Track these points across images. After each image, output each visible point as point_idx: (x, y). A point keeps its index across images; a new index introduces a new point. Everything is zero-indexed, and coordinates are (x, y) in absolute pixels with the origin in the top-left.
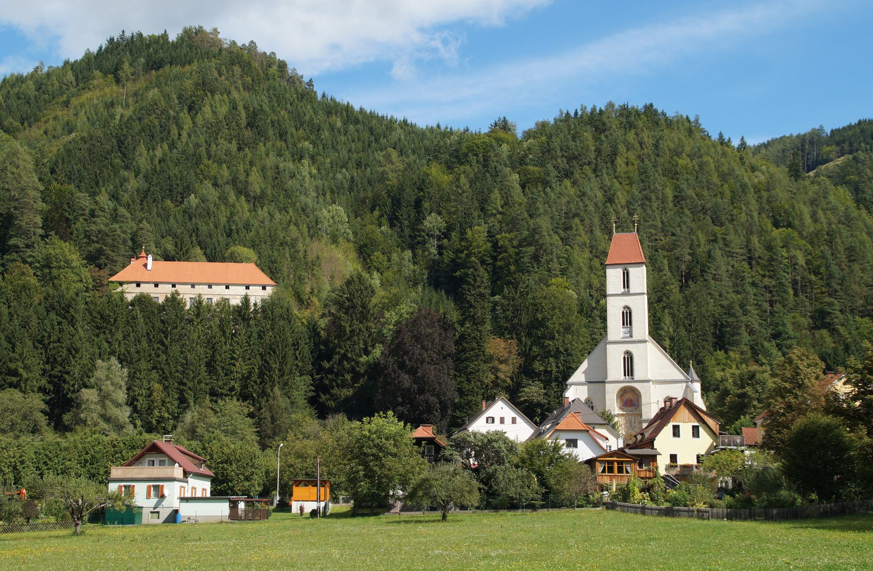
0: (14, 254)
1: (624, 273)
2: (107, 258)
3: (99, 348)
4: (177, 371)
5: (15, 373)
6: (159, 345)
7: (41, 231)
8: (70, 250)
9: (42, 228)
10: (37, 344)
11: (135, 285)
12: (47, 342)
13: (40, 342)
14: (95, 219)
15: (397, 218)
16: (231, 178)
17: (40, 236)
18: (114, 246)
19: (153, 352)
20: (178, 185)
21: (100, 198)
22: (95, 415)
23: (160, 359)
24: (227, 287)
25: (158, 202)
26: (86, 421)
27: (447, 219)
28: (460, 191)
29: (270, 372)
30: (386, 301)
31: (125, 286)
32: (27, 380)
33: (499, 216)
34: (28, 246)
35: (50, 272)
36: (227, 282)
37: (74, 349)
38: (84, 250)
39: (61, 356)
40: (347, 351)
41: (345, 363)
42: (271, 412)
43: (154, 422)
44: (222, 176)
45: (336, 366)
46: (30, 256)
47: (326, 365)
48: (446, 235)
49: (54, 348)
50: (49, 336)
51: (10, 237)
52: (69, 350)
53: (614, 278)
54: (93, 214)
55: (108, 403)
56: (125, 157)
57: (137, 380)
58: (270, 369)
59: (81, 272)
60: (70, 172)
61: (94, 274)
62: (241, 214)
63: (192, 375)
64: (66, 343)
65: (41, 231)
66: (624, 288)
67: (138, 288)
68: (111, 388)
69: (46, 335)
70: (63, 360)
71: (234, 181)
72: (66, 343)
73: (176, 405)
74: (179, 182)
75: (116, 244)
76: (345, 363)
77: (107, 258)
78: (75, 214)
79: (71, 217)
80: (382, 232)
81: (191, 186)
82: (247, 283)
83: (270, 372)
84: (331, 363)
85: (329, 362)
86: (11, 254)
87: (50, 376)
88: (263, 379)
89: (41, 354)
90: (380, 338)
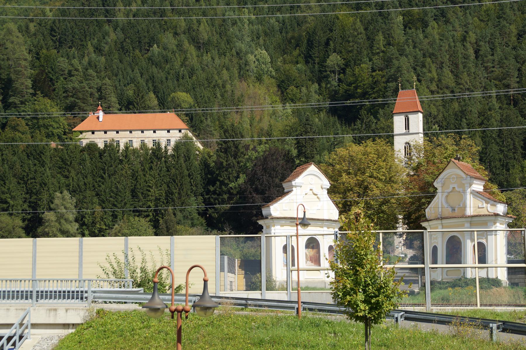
0: (13, 109)
1: (406, 119)
2: (79, 108)
3: (59, 183)
4: (111, 197)
5: (6, 202)
6: (100, 179)
7: (31, 91)
8: (51, 106)
9: (32, 88)
10: (20, 181)
11: (91, 133)
12: (26, 179)
13: (22, 180)
14: (72, 78)
15: (310, 57)
16: (187, 28)
17: (31, 94)
18: (84, 99)
19: (95, 184)
20: (145, 37)
21: (75, 61)
22: (55, 229)
23: (101, 188)
24: (154, 132)
25: (129, 52)
26: (49, 233)
27: (345, 57)
28: (356, 33)
29: (172, 195)
30: (288, 128)
31: (84, 134)
32: (13, 206)
33: (381, 54)
34: (22, 103)
35: (38, 122)
36: (154, 128)
37: (44, 183)
38: (63, 103)
39: (35, 189)
40: (224, 179)
41: (223, 187)
42: (166, 224)
43: (96, 231)
44: (180, 27)
45: (218, 189)
46: (24, 111)
47: (212, 189)
48: (343, 71)
49: (31, 183)
50: (28, 175)
51: (10, 97)
52: (41, 185)
53: (398, 122)
54: (70, 74)
55: (63, 221)
56: (108, 13)
57: (85, 204)
58: (172, 194)
59: (59, 120)
60: (65, 29)
61: (70, 121)
62: (190, 60)
63: (120, 200)
64: (38, 180)
65: (31, 91)
66: (406, 129)
67: (93, 135)
68: (64, 211)
69: (25, 174)
70: (37, 191)
71: (189, 29)
72: (38, 180)
73: (111, 220)
74: (146, 34)
75: (85, 97)
76: (223, 187)
77: (79, 108)
78: (57, 75)
79: (54, 78)
80: (298, 69)
81: (155, 37)
82: (168, 128)
83: (172, 195)
84: (215, 187)
85: (213, 186)
86: (11, 109)
87: (30, 202)
88: (168, 200)
89: (23, 187)
90: (243, 169)
